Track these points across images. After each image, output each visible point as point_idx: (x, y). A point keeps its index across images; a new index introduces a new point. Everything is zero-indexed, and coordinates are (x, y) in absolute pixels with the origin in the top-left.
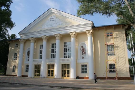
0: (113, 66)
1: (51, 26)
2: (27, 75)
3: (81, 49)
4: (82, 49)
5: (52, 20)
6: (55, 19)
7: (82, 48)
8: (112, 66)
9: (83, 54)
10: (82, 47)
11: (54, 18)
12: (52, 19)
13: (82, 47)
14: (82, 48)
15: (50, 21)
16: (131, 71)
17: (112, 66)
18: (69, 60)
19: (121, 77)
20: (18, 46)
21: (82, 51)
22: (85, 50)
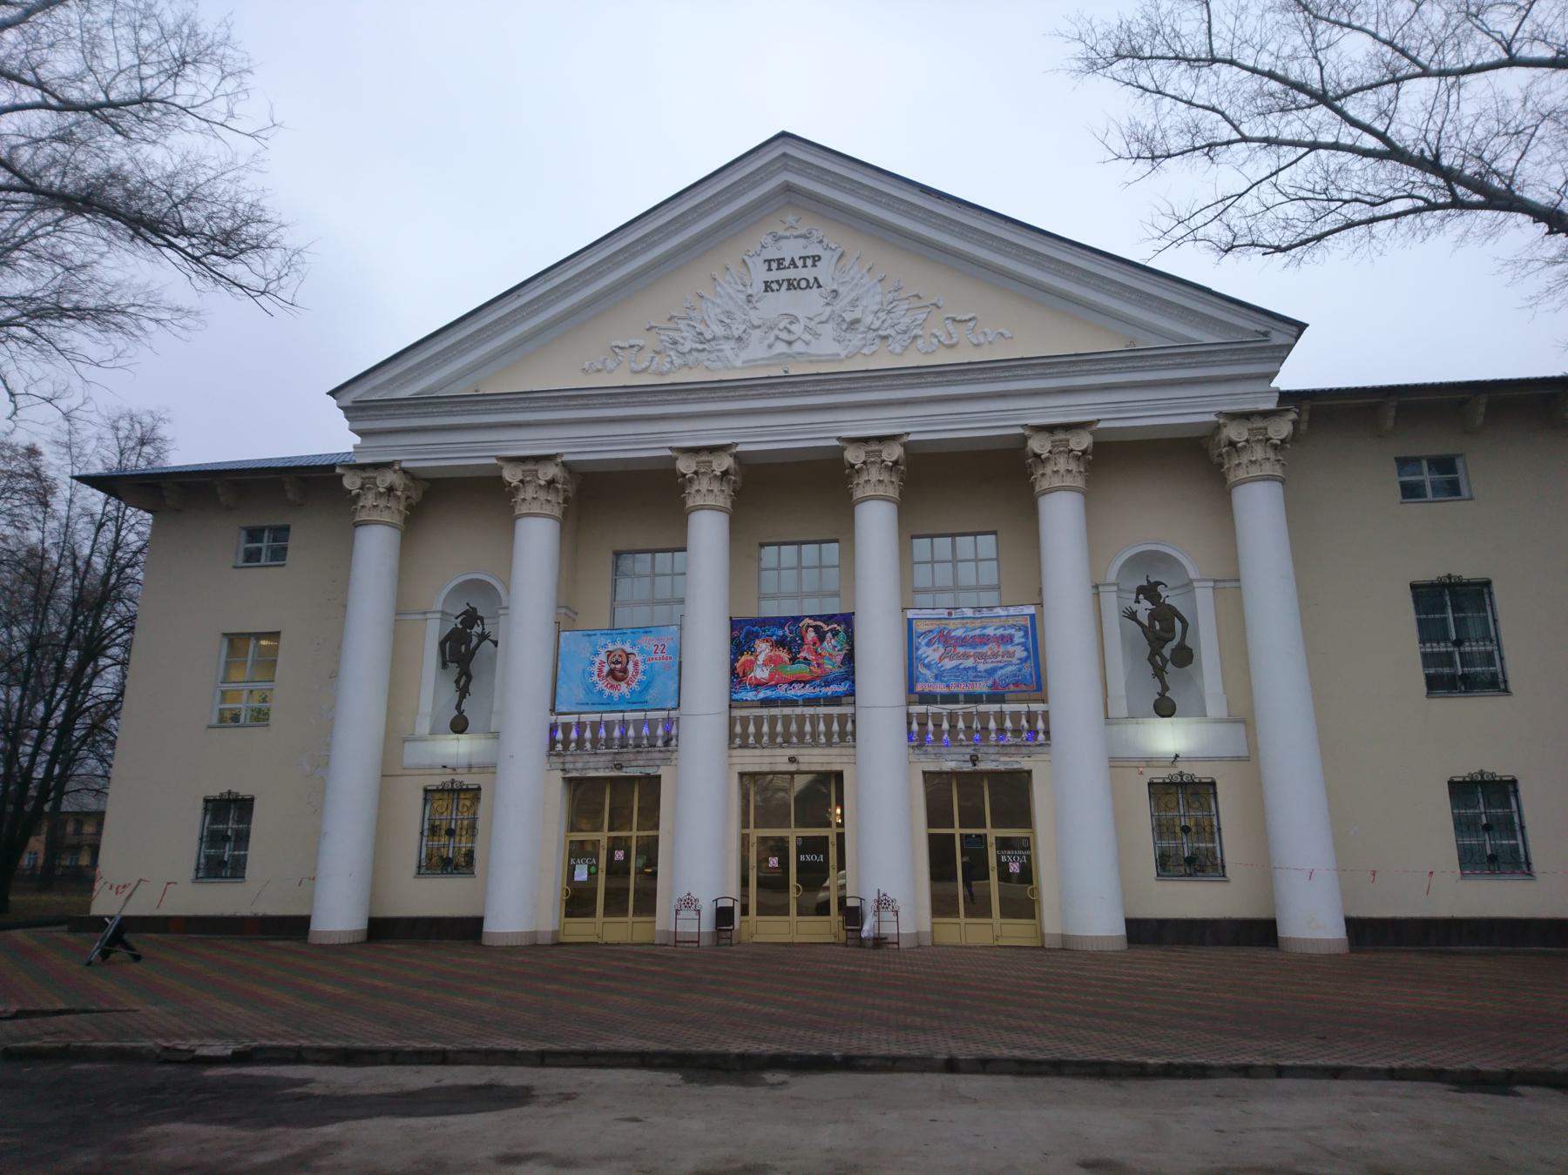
0: (964, 838)
1: (781, 348)
2: (304, 912)
3: (1132, 616)
4: (1143, 617)
5: (792, 285)
6: (823, 271)
7: (1144, 608)
8: (952, 826)
9: (1159, 672)
10: (1149, 591)
11: (816, 259)
12: (791, 274)
13: (1140, 590)
14: (1144, 608)
15: (768, 286)
16: (879, 942)
17: (952, 826)
18: (808, 728)
19: (561, 1070)
20: (279, 555)
21: (1147, 631)
22: (1178, 625)
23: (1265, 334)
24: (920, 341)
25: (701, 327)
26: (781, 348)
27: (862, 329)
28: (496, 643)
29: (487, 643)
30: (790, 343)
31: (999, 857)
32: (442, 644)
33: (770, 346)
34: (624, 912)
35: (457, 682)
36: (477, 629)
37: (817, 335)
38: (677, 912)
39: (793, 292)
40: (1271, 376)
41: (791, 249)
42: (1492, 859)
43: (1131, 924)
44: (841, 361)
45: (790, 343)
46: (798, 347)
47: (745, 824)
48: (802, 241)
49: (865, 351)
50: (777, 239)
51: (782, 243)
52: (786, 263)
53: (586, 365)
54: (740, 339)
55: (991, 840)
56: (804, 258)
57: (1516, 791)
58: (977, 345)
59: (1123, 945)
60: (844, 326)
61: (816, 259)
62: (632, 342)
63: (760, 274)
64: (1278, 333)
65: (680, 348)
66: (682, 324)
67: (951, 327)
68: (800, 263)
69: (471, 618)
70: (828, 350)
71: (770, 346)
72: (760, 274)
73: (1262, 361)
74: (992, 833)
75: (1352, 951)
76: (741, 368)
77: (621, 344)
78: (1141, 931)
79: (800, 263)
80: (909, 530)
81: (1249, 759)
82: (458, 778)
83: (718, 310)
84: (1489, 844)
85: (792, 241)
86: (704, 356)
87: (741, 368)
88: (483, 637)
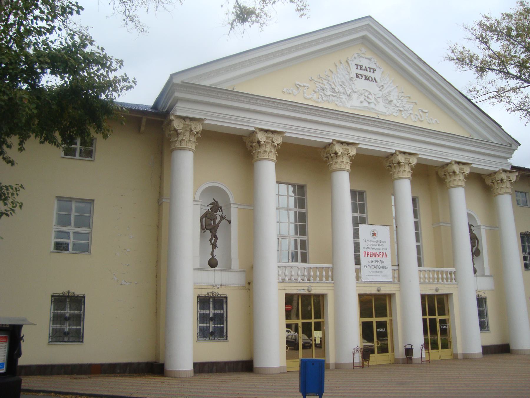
1: (365, 104)
5: (367, 78)
6: (377, 75)
11: (374, 70)
23: (511, 145)
24: (412, 116)
25: (333, 86)
26: (365, 104)
27: (393, 105)
28: (230, 222)
29: (224, 221)
30: (369, 103)
31: (440, 327)
32: (201, 219)
33: (362, 102)
34: (437, 348)
35: (211, 240)
36: (219, 213)
37: (378, 102)
38: (353, 354)
39: (366, 81)
40: (507, 158)
41: (365, 63)
42: (212, 334)
43: (195, 364)
44: (386, 116)
45: (369, 103)
46: (372, 106)
47: (424, 314)
48: (368, 61)
49: (394, 114)
50: (360, 57)
51: (361, 59)
52: (364, 68)
53: (285, 90)
54: (349, 95)
55: (438, 321)
56: (370, 68)
57: (485, 301)
58: (429, 123)
59: (192, 374)
60: (387, 102)
61: (374, 70)
62: (305, 84)
63: (354, 71)
64: (512, 144)
65: (326, 93)
66: (325, 82)
67: (421, 113)
68: (368, 70)
69: (215, 207)
70: (381, 110)
71: (362, 102)
72: (354, 71)
73: (506, 152)
74: (438, 318)
75: (194, 375)
76: (350, 109)
77: (300, 84)
78: (201, 368)
79: (368, 70)
80: (517, 203)
81: (250, 286)
82: (216, 291)
83: (340, 80)
84: (211, 326)
85: (364, 59)
86: (335, 99)
87: (350, 109)
88: (222, 218)
